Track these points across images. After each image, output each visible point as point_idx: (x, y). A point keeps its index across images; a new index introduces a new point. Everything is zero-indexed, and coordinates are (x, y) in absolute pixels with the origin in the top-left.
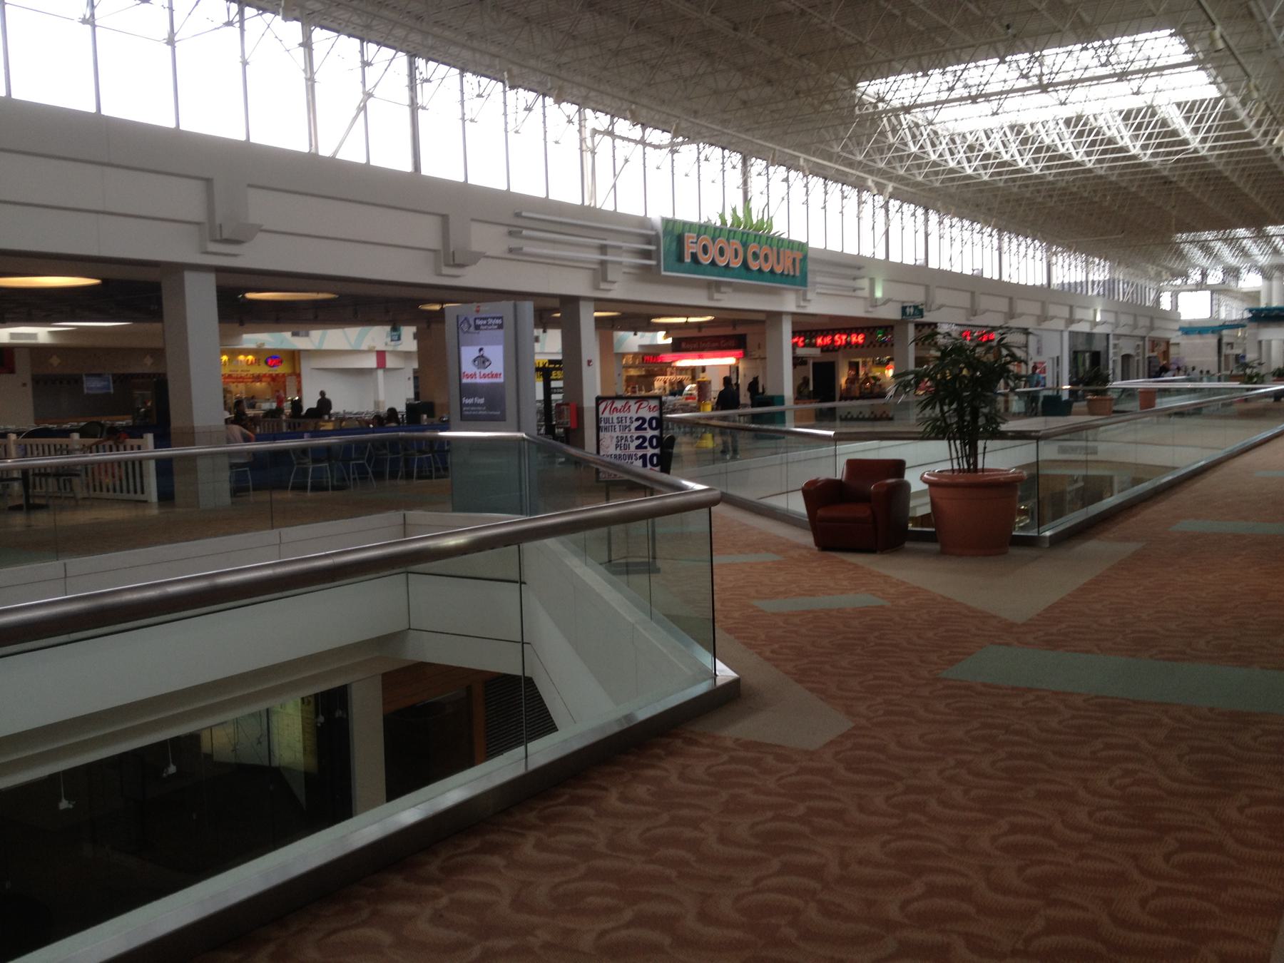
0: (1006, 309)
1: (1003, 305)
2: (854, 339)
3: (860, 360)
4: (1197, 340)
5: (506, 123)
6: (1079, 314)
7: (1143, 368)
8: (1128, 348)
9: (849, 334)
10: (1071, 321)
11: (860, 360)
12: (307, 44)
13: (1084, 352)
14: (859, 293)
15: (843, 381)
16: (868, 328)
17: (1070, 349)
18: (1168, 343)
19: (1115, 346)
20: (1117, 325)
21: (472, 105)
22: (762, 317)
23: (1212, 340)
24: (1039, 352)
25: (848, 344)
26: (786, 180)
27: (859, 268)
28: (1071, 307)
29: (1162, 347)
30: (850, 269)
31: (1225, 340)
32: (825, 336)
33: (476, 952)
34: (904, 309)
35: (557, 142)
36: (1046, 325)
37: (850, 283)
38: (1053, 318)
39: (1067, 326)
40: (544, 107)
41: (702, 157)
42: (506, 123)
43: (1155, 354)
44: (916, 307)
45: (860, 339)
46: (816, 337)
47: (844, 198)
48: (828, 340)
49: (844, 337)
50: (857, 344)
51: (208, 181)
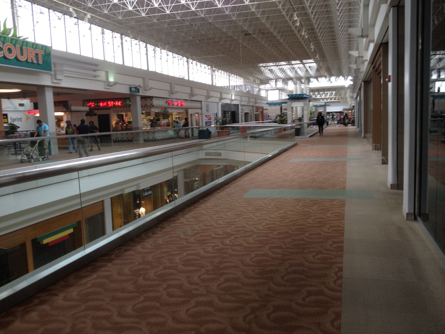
0: (219, 96)
1: (188, 90)
2: (117, 104)
3: (124, 114)
4: (273, 108)
5: (33, 19)
6: (224, 96)
7: (253, 117)
8: (247, 110)
9: (114, 102)
10: (221, 99)
11: (124, 114)
12: (103, 33)
13: (228, 111)
14: (98, 78)
15: (113, 123)
16: (123, 98)
17: (222, 111)
18: (263, 108)
19: (242, 109)
20: (241, 101)
21: (37, 17)
22: (35, 89)
23: (278, 107)
24: (207, 111)
25: (114, 106)
26: (90, 29)
27: (96, 65)
28: (221, 93)
29: (261, 110)
30: (90, 66)
31: (283, 108)
32: (104, 102)
33: (41, 330)
34: (130, 88)
35: (55, 27)
36: (210, 100)
37: (93, 73)
38: (212, 97)
39: (220, 101)
40: (64, 18)
41: (114, 37)
42: (33, 19)
43: (258, 113)
44: (136, 88)
45: (120, 103)
46: (99, 102)
47: (168, 55)
48: (105, 104)
49: (112, 103)
50: (118, 106)
51: (144, 78)
